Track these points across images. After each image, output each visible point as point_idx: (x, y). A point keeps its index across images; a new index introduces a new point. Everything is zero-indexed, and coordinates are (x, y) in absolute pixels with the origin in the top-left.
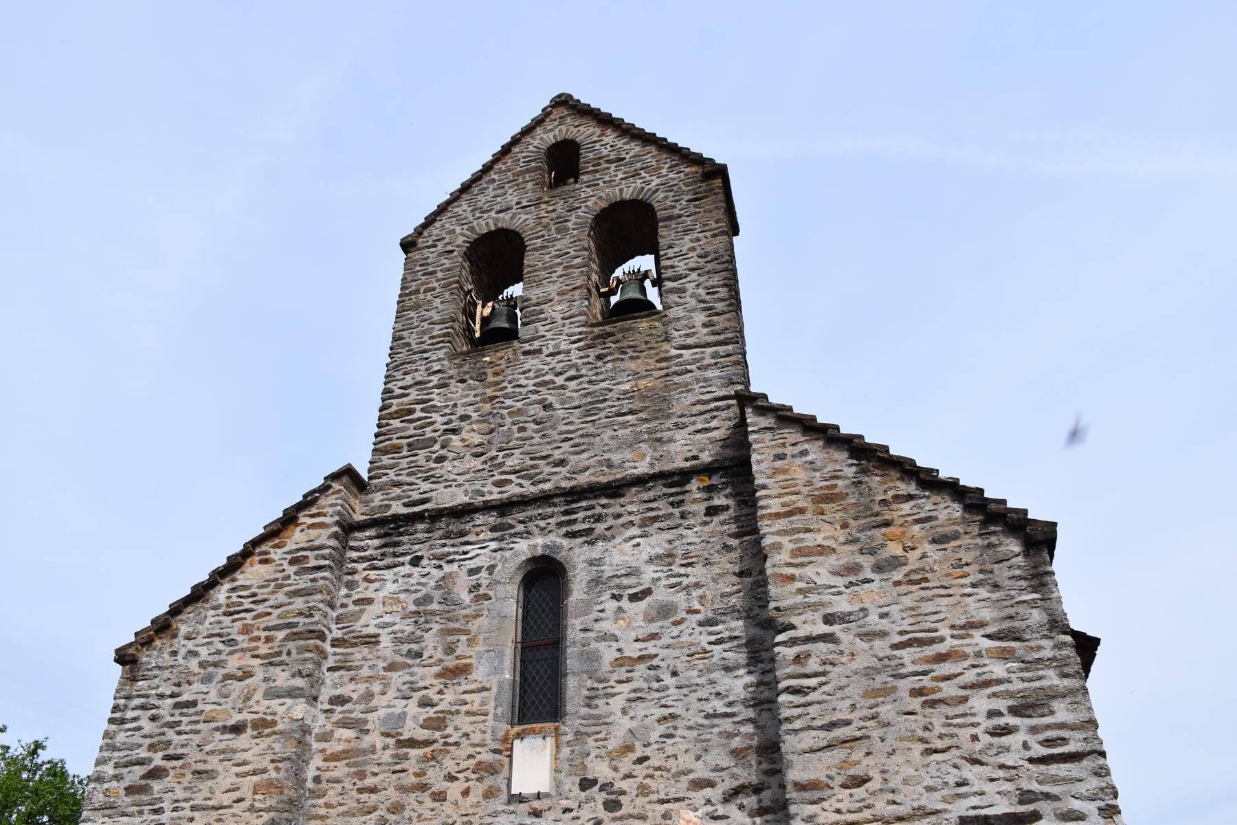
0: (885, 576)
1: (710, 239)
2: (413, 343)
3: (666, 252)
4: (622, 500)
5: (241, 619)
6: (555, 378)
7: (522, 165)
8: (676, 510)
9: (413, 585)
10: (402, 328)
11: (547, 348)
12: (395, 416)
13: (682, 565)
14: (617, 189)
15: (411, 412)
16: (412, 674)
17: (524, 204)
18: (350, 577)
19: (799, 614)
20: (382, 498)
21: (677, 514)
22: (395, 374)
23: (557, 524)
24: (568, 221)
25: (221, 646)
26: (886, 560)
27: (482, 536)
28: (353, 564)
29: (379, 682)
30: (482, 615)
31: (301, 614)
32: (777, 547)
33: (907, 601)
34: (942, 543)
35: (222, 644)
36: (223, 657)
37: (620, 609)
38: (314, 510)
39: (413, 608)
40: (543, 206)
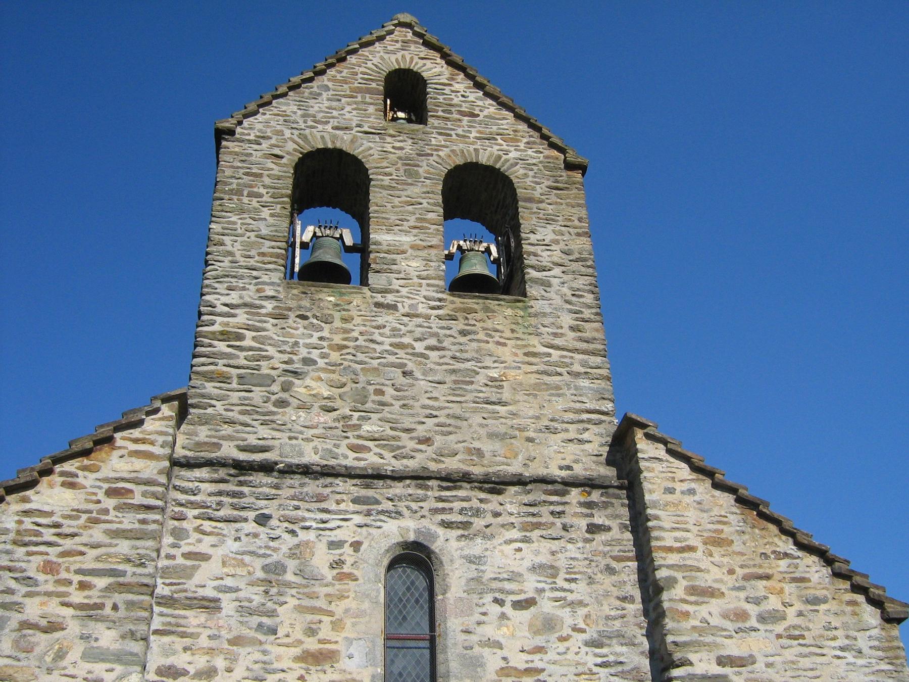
0: (769, 627)
1: (574, 237)
2: (238, 254)
3: (527, 235)
4: (500, 498)
5: (41, 553)
6: (413, 343)
7: (360, 81)
8: (557, 520)
9: (260, 547)
10: (222, 231)
11: (403, 306)
12: (221, 337)
13: (566, 580)
14: (472, 148)
15: (240, 337)
16: (265, 652)
17: (366, 129)
18: (176, 523)
19: (696, 652)
20: (209, 433)
21: (559, 525)
22: (216, 285)
23: (430, 510)
24: (418, 166)
25: (13, 584)
26: (769, 612)
27: (343, 506)
28: (181, 509)
29: (222, 656)
30: (348, 597)
31: (128, 561)
32: (672, 581)
33: (789, 655)
34: (815, 604)
35: (13, 581)
36: (17, 598)
37: (503, 616)
38: (136, 433)
39: (260, 574)
40: (389, 139)
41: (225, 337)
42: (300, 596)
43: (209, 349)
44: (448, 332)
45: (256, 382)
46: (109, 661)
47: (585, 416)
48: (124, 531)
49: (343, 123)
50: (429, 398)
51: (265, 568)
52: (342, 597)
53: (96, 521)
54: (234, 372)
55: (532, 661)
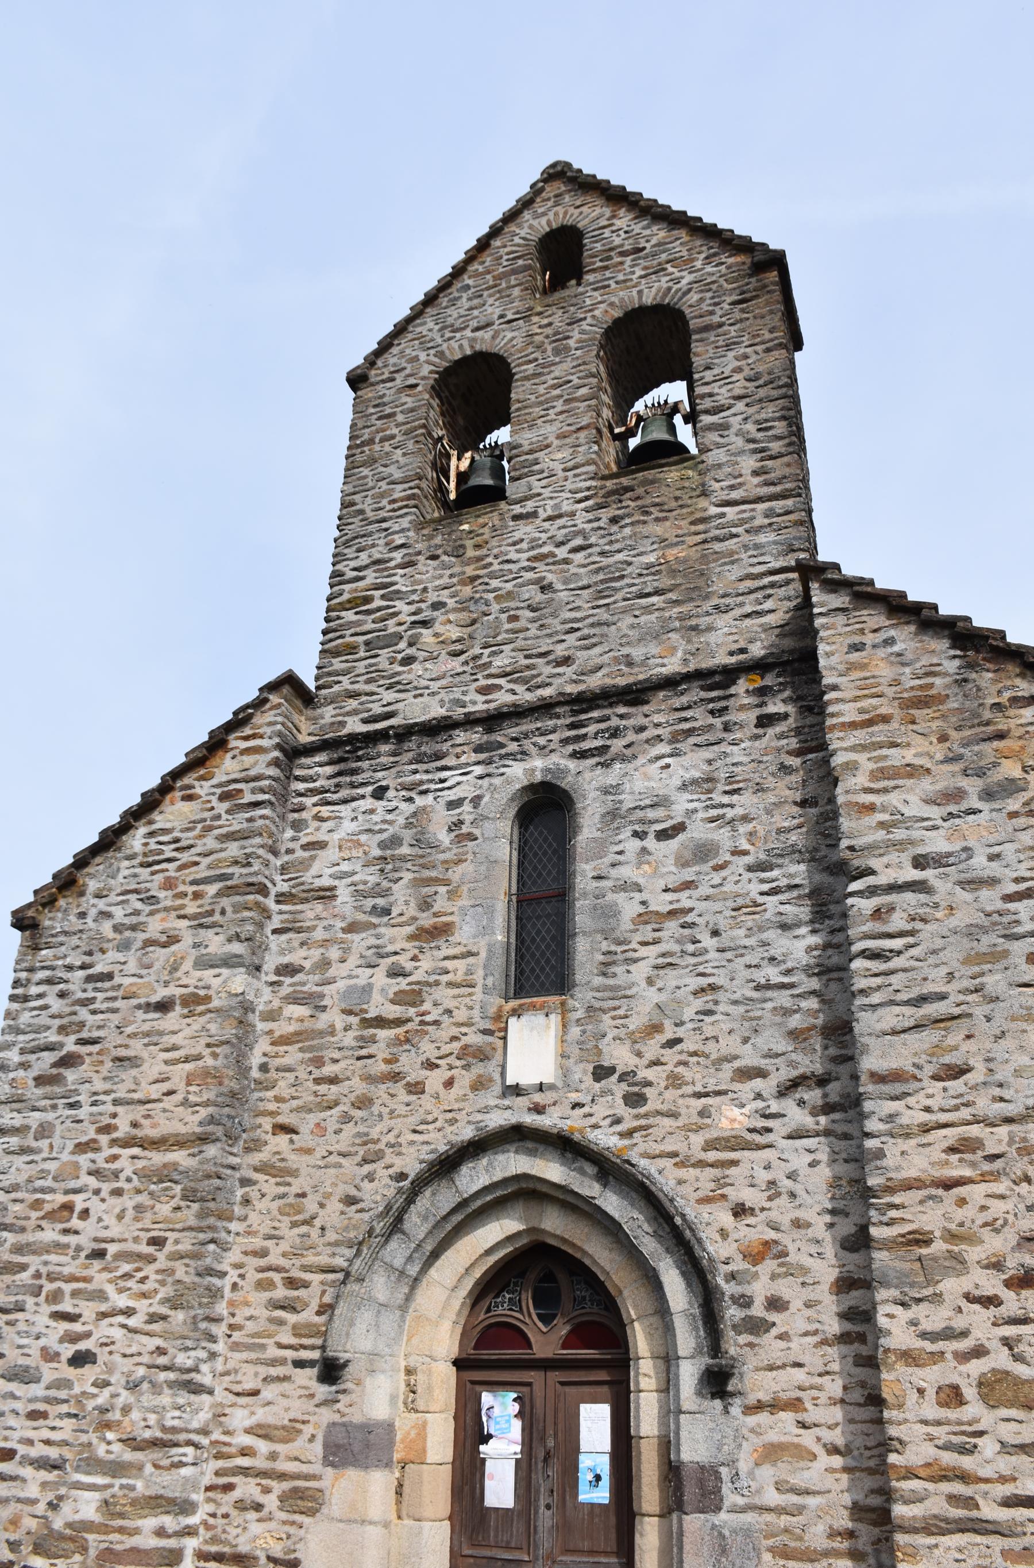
0: (997, 805)
1: (762, 355)
2: (368, 510)
4: (646, 708)
5: (163, 871)
9: (376, 823)
12: (348, 606)
13: (726, 792)
14: (635, 291)
15: (368, 600)
16: (378, 936)
17: (510, 317)
18: (296, 815)
21: (720, 726)
23: (561, 741)
24: (568, 337)
25: (139, 905)
26: (999, 784)
27: (463, 759)
28: (300, 799)
31: (236, 863)
36: (142, 919)
37: (644, 850)
38: (248, 731)
39: (377, 852)
40: (535, 319)
42: (415, 868)
44: (595, 525)
45: (381, 644)
47: (766, 580)
48: (233, 833)
49: (483, 321)
51: (382, 845)
52: (459, 862)
53: (210, 829)
54: (361, 639)
55: (678, 901)
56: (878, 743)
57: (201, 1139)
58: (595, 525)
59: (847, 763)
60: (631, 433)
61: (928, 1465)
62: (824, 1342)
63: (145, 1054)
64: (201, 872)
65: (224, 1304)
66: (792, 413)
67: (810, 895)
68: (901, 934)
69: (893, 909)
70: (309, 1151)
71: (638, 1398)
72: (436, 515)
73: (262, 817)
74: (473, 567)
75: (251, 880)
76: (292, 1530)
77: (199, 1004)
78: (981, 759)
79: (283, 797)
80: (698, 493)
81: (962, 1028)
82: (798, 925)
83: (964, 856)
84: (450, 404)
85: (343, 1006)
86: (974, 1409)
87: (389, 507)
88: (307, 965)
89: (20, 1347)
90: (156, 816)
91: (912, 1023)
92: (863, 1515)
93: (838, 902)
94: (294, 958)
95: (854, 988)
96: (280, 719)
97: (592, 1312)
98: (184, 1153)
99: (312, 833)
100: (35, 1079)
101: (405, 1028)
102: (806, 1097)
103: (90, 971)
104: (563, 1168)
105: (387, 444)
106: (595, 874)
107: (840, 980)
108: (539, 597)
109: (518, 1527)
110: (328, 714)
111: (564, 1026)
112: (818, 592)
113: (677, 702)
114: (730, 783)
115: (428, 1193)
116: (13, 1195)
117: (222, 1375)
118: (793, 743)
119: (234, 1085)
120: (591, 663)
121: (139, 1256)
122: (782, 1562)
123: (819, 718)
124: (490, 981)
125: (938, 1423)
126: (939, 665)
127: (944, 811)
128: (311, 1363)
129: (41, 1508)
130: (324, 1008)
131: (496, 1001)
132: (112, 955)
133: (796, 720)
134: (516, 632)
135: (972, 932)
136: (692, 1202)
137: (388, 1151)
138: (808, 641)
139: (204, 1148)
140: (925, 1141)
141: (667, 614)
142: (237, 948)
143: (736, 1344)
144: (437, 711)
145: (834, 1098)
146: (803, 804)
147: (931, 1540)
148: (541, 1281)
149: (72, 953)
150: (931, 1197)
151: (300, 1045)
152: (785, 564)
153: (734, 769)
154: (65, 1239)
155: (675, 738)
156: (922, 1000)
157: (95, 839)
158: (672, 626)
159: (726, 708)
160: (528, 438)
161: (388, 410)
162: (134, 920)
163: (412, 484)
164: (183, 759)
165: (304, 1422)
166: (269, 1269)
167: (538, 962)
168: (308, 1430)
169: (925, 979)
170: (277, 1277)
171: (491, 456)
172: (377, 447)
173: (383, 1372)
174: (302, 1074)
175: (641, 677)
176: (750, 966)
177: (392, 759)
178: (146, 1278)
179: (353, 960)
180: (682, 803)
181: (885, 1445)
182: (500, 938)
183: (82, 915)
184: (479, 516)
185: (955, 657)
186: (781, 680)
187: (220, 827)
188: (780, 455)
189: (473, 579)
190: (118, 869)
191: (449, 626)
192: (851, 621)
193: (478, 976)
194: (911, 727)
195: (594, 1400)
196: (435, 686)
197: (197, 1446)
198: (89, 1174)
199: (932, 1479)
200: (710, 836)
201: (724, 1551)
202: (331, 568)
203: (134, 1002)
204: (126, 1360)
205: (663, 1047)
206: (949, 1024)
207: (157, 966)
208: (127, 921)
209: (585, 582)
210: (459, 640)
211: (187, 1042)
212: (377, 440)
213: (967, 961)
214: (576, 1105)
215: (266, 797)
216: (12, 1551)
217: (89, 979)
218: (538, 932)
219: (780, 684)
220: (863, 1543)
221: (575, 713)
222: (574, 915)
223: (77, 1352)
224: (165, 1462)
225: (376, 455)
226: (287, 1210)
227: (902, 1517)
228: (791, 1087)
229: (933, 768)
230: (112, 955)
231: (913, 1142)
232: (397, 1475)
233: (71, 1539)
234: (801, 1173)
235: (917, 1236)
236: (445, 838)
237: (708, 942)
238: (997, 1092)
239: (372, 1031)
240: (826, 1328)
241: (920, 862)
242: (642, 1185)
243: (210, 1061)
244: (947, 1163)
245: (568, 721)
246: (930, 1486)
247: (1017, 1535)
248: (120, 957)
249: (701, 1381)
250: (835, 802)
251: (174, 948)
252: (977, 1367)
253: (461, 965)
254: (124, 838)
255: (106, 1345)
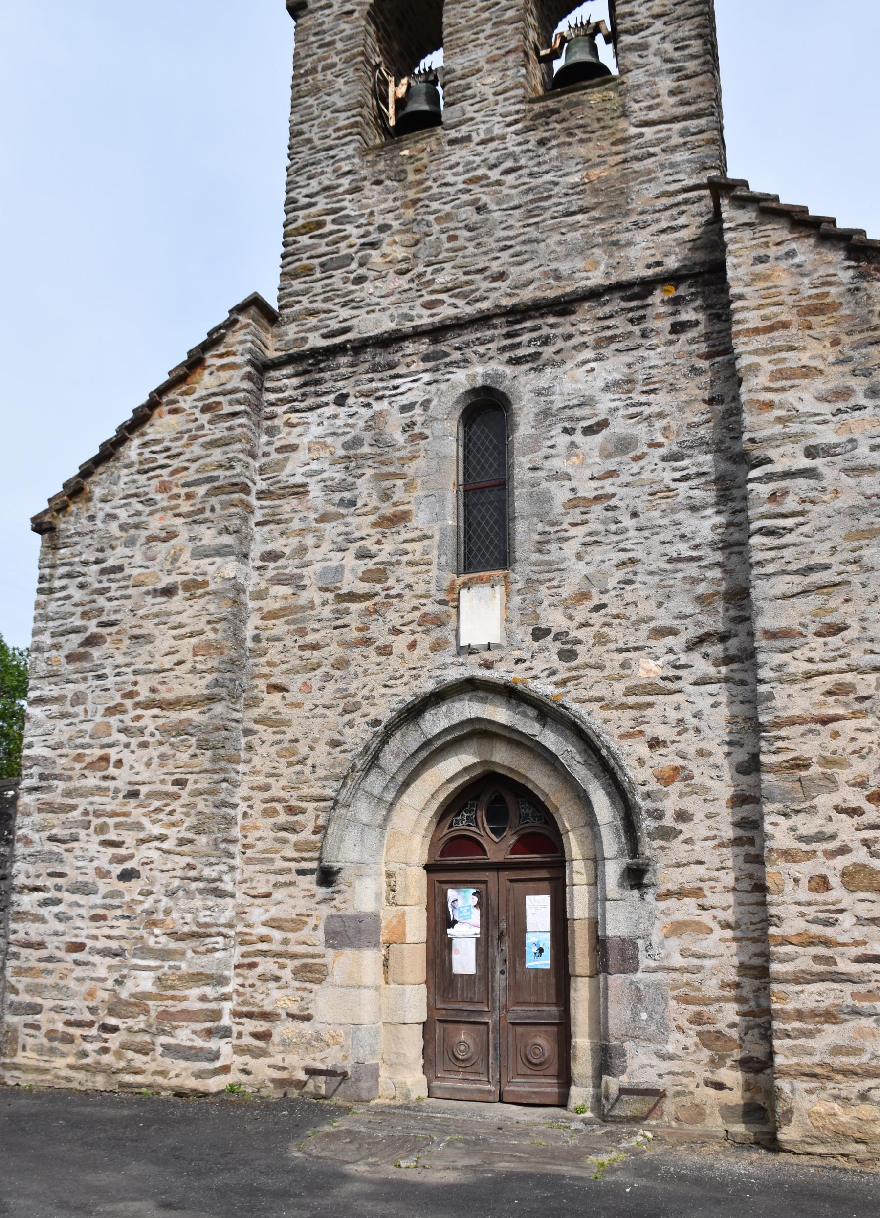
2: (315, 138)
4: (573, 318)
5: (158, 476)
9: (340, 427)
11: (478, 134)
12: (303, 231)
13: (644, 392)
15: (320, 225)
16: (346, 525)
18: (269, 423)
23: (499, 349)
25: (140, 507)
27: (413, 368)
28: (272, 408)
29: (311, 535)
31: (220, 466)
36: (143, 518)
37: (573, 444)
38: (222, 350)
39: (341, 452)
41: (307, 229)
42: (376, 465)
43: (294, 246)
44: (525, 147)
45: (335, 265)
46: (211, 556)
47: (681, 197)
48: (216, 440)
50: (504, 229)
51: (346, 446)
53: (194, 438)
54: (316, 261)
56: (778, 347)
57: (209, 699)
58: (525, 147)
59: (750, 365)
60: (556, 55)
61: (799, 934)
62: (721, 845)
63: (156, 632)
64: (191, 475)
65: (238, 829)
66: (708, 31)
67: (716, 481)
68: (793, 514)
69: (787, 492)
70: (298, 705)
71: (572, 890)
72: (378, 141)
73: (240, 425)
74: (414, 190)
75: (234, 481)
76: (305, 994)
77: (198, 588)
78: (868, 361)
79: (257, 407)
80: (618, 114)
81: (843, 591)
82: (705, 507)
83: (849, 446)
84: (385, 30)
85: (320, 585)
86: (838, 893)
87: (334, 135)
88: (287, 551)
89: (78, 868)
90: (147, 428)
91: (800, 589)
92: (748, 971)
93: (739, 487)
94: (276, 546)
95: (752, 560)
96: (249, 337)
97: (534, 825)
98: (196, 711)
99: (284, 437)
100: (67, 657)
101: (373, 601)
102: (710, 651)
103: (104, 565)
104: (509, 712)
105: (329, 72)
106: (531, 465)
107: (740, 553)
108: (476, 218)
109: (479, 987)
110: (291, 331)
111: (507, 595)
112: (727, 208)
113: (601, 312)
114: (648, 384)
115: (398, 735)
116: (59, 752)
117: (240, 883)
118: (703, 347)
119: (233, 654)
120: (523, 278)
121: (167, 795)
122: (684, 1006)
123: (726, 325)
124: (443, 559)
125: (809, 904)
126: (835, 275)
127: (833, 407)
128: (311, 872)
129: (110, 984)
130: (304, 587)
131: (449, 577)
132: (121, 551)
133: (705, 327)
134: (456, 251)
135: (854, 512)
136: (616, 737)
137: (364, 702)
138: (718, 254)
139: (212, 706)
140: (807, 686)
141: (591, 231)
142: (227, 539)
143: (651, 848)
144: (386, 325)
145: (733, 651)
146: (711, 401)
147: (799, 988)
148: (492, 803)
149: (87, 551)
150: (810, 731)
151: (286, 619)
152: (698, 182)
153: (651, 371)
154: (105, 784)
155: (598, 345)
156: (810, 569)
157: (97, 451)
158: (595, 242)
159: (644, 317)
160: (460, 63)
161: (328, 39)
162: (137, 519)
163: (354, 112)
164: (167, 378)
165: (308, 916)
166: (273, 800)
167: (483, 542)
168: (311, 922)
169: (812, 552)
170: (278, 806)
171: (426, 81)
172: (320, 76)
173: (369, 876)
174: (289, 643)
175: (568, 290)
176: (664, 543)
177: (350, 370)
178: (174, 811)
179: (326, 546)
180: (605, 403)
181: (767, 921)
182: (450, 523)
183: (92, 518)
184: (417, 142)
185: (849, 268)
186: (693, 290)
187: (204, 436)
188: (696, 75)
189: (415, 202)
190: (119, 477)
191: (394, 248)
192: (757, 235)
193: (434, 555)
194: (807, 332)
195: (537, 893)
196: (385, 302)
197: (225, 936)
198: (119, 731)
199: (802, 945)
200: (629, 431)
201: (639, 1000)
202: (285, 196)
203: (143, 589)
204: (163, 874)
205: (590, 611)
206: (831, 590)
207: (160, 558)
208: (131, 521)
209: (516, 202)
210: (405, 260)
211: (191, 620)
212: (319, 69)
213: (848, 537)
214: (519, 661)
215: (243, 407)
216: (92, 1013)
217: (103, 572)
218: (483, 517)
219: (692, 294)
220: (746, 992)
221: (510, 323)
222: (514, 501)
223: (124, 870)
224: (202, 949)
225: (320, 84)
226: (284, 753)
227: (778, 972)
228: (697, 643)
229: (826, 369)
230: (121, 551)
231: (798, 687)
232: (384, 952)
233: (135, 1005)
234: (705, 712)
235: (799, 762)
236: (400, 438)
237: (628, 522)
238: (869, 646)
239: (345, 605)
240: (723, 834)
241: (811, 452)
242: (574, 724)
243: (211, 636)
244: (825, 703)
245: (505, 331)
246: (800, 950)
247: (864, 982)
248: (128, 552)
249: (622, 876)
250: (739, 400)
251: (173, 542)
252: (841, 862)
253: (418, 546)
254: (121, 449)
255: (147, 863)
